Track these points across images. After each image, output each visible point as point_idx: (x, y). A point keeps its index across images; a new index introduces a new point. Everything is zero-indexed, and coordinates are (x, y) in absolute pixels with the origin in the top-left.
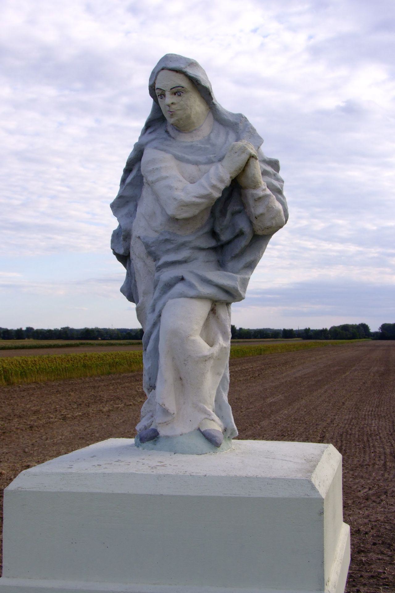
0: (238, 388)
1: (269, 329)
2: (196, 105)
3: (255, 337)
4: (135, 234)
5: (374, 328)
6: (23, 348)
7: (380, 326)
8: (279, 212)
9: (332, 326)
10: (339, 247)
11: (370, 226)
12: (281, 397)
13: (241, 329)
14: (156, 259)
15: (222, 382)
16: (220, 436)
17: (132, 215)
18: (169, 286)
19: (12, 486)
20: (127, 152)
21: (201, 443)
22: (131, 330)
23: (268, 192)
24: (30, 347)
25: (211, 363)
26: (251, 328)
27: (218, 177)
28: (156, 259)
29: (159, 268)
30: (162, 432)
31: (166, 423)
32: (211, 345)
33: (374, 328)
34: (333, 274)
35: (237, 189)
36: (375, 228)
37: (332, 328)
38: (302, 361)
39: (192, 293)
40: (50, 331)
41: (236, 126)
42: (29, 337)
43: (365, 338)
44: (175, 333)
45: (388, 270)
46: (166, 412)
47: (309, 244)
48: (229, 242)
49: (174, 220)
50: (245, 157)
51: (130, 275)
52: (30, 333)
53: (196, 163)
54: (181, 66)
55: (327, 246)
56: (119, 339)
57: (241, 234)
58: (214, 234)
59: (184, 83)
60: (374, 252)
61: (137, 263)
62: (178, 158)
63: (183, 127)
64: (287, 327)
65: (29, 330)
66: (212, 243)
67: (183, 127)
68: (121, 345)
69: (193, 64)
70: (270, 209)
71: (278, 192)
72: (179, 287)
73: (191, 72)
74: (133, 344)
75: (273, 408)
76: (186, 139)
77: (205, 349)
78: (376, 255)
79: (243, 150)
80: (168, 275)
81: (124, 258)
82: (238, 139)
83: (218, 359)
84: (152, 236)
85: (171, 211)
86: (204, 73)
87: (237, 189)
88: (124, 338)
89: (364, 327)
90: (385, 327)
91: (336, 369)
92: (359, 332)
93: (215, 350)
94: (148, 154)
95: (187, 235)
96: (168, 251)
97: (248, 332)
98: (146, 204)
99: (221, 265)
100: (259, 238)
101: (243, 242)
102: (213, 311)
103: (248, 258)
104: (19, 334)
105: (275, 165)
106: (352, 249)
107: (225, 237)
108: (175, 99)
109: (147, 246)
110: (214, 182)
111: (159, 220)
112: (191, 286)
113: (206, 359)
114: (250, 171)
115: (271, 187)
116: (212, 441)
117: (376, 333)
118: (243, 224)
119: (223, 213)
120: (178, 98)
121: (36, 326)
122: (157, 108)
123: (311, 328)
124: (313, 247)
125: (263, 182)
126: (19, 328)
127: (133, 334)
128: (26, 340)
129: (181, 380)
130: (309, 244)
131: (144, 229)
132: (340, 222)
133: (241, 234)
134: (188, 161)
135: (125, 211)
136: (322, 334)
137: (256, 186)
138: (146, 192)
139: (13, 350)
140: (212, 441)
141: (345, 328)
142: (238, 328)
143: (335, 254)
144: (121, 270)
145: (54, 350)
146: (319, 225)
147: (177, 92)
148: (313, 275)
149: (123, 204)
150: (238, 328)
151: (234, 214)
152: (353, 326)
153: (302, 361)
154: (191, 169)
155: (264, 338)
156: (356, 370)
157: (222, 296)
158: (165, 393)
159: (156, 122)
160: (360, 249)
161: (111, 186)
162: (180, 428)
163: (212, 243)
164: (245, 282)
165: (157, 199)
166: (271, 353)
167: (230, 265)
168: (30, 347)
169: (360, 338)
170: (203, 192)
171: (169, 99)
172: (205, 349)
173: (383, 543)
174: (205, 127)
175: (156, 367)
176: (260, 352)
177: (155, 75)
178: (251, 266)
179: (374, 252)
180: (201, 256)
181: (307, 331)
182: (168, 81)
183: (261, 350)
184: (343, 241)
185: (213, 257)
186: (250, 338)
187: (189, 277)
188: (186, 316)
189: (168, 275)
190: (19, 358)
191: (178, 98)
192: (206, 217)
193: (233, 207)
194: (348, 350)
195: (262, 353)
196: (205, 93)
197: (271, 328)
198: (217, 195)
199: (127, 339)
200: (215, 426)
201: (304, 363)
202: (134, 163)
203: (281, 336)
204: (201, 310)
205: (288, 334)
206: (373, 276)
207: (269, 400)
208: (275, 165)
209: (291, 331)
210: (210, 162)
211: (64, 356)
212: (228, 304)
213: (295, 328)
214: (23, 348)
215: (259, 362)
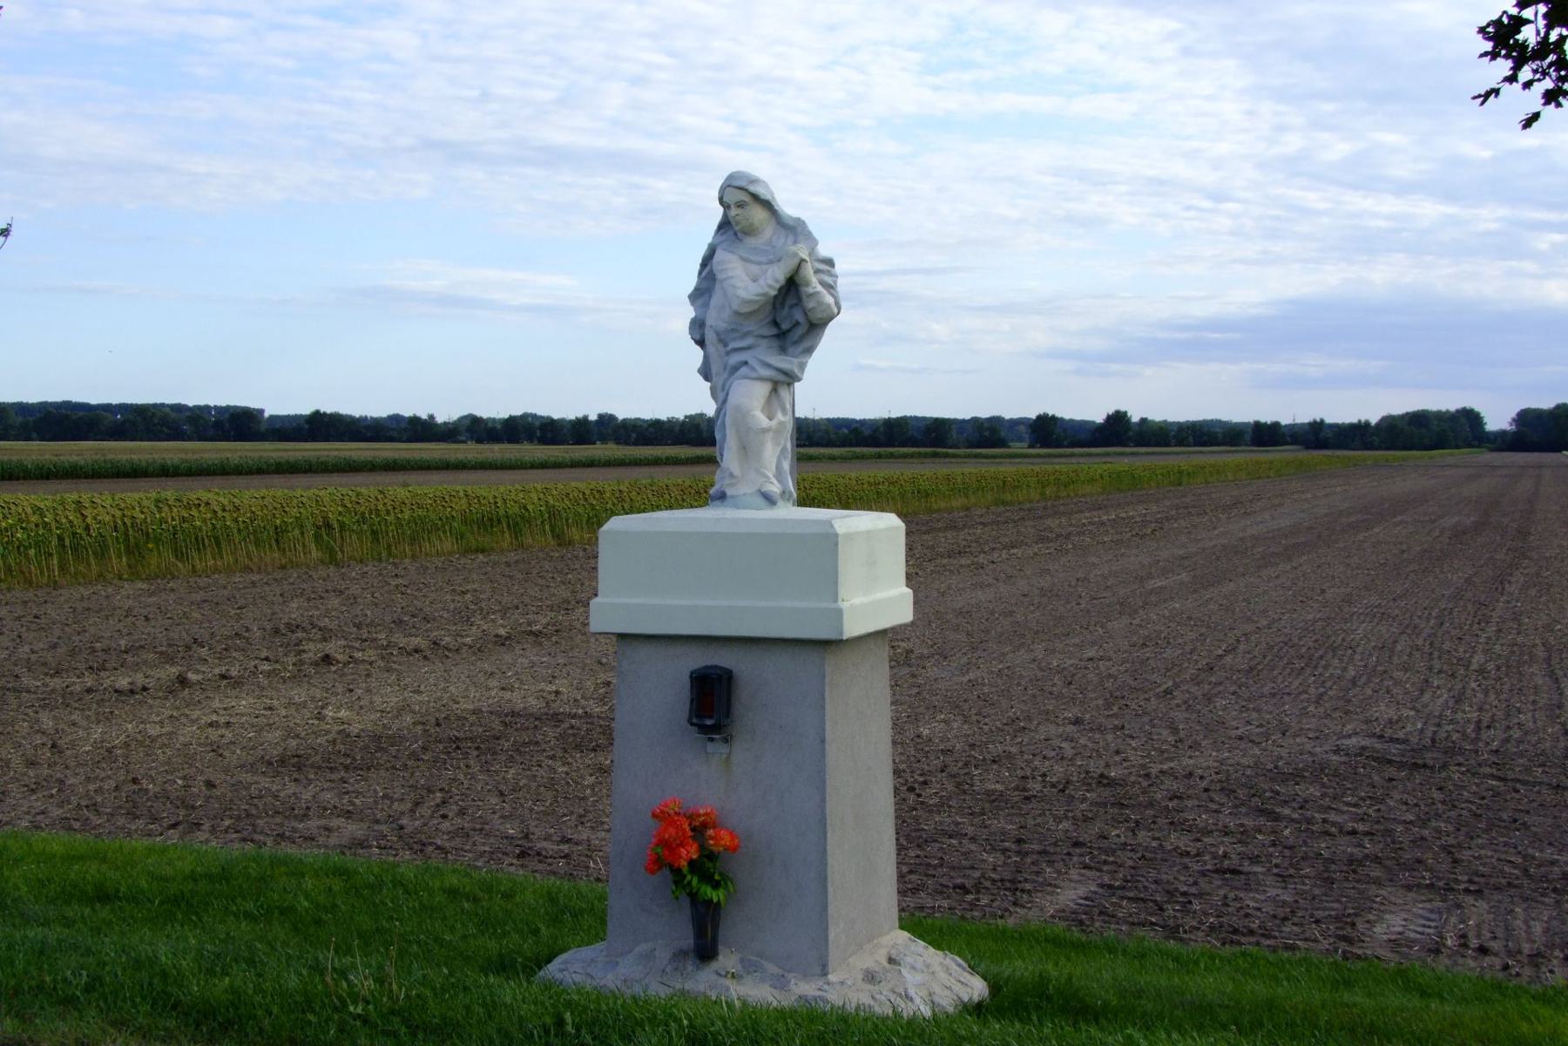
0: (1093, 559)
1: (1219, 422)
2: (758, 215)
3: (1181, 443)
4: (709, 322)
5: (1498, 419)
6: (591, 464)
7: (1513, 414)
8: (829, 306)
9: (1385, 413)
10: (1391, 205)
11: (1468, 149)
12: (1184, 576)
13: (1144, 421)
14: (726, 345)
15: (784, 450)
16: (777, 497)
17: (706, 305)
18: (735, 369)
19: (606, 527)
20: (702, 250)
21: (760, 501)
22: (863, 422)
23: (820, 288)
24: (609, 464)
25: (771, 434)
26: (1170, 419)
27: (775, 277)
28: (726, 345)
29: (728, 353)
30: (729, 493)
31: (732, 485)
32: (770, 419)
33: (1498, 419)
34: (1382, 276)
35: (792, 286)
36: (1486, 154)
37: (1384, 419)
38: (1276, 501)
39: (754, 375)
40: (656, 424)
41: (795, 229)
42: (604, 440)
43: (1470, 446)
44: (738, 408)
45: (1529, 266)
46: (732, 475)
47: (1313, 199)
48: (789, 331)
49: (737, 313)
50: (796, 261)
51: (706, 357)
52: (607, 429)
53: (759, 263)
54: (742, 184)
55: (1359, 202)
56: (829, 444)
57: (797, 324)
58: (775, 323)
59: (746, 198)
60: (1489, 217)
61: (711, 349)
62: (744, 260)
63: (750, 231)
64: (1267, 417)
65: (606, 420)
66: (774, 331)
67: (750, 231)
68: (832, 458)
69: (755, 181)
70: (820, 303)
71: (830, 288)
72: (744, 370)
73: (752, 188)
74: (862, 457)
75: (1153, 598)
76: (751, 241)
77: (763, 421)
78: (1493, 226)
79: (795, 255)
80: (735, 359)
81: (701, 343)
82: (795, 242)
83: (778, 431)
84: (722, 325)
85: (735, 307)
86: (766, 186)
87: (792, 286)
88: (844, 443)
89: (1470, 418)
90: (1527, 419)
91: (1352, 519)
92: (1461, 429)
93: (774, 423)
94: (720, 255)
95: (750, 326)
96: (734, 339)
97: (1161, 428)
98: (716, 300)
99: (783, 350)
100: (815, 326)
101: (800, 331)
102: (775, 390)
103: (806, 344)
104: (582, 431)
105: (830, 262)
106: (1429, 210)
107: (785, 326)
108: (739, 211)
109: (718, 334)
110: (770, 282)
111: (727, 314)
112: (753, 369)
113: (765, 431)
114: (802, 271)
115: (822, 283)
116: (769, 500)
117: (1503, 433)
118: (798, 316)
119: (783, 305)
120: (745, 210)
121: (623, 412)
122: (725, 215)
123: (1328, 420)
124: (1322, 206)
125: (814, 280)
126: (580, 415)
127: (867, 433)
128: (598, 445)
129: (744, 449)
130: (1313, 199)
131: (715, 320)
132: (1391, 138)
133: (797, 324)
134: (752, 262)
135: (701, 301)
136: (1355, 436)
137: (808, 284)
138: (717, 286)
139: (567, 470)
140: (769, 500)
141: (1419, 419)
142: (1135, 419)
143: (1382, 224)
144: (697, 354)
145: (668, 469)
146: (1338, 149)
147: (740, 205)
148: (1326, 279)
149: (701, 294)
150: (1135, 419)
151: (792, 307)
152: (1440, 416)
153: (1276, 501)
154: (754, 269)
155: (1204, 444)
156: (1401, 522)
157: (781, 377)
158: (730, 459)
159: (725, 225)
160: (1451, 210)
161: (691, 281)
162: (744, 489)
163: (774, 331)
164: (802, 367)
165: (725, 294)
166: (1207, 482)
167: (791, 350)
168: (609, 464)
169: (1457, 447)
170: (761, 291)
171: (733, 212)
172: (763, 421)
173: (1222, 789)
174: (769, 231)
175: (724, 437)
176: (1179, 478)
177: (722, 190)
178: (809, 351)
179: (1489, 217)
180: (764, 343)
181: (1317, 427)
182: (732, 197)
183: (1180, 472)
184: (1403, 189)
185: (775, 343)
186: (1167, 445)
187: (752, 362)
188: (751, 395)
189: (735, 359)
190: (582, 486)
191: (745, 210)
192: (769, 307)
193: (790, 301)
194: (1410, 475)
195: (1185, 480)
196: (768, 205)
197: (1224, 419)
198: (773, 293)
199: (851, 445)
200: (774, 488)
201: (1281, 505)
202: (707, 261)
203: (1248, 437)
204: (762, 390)
205: (1266, 435)
206: (1491, 284)
207: (1151, 584)
208: (830, 262)
209: (1276, 426)
210: (770, 262)
211: (688, 483)
212: (789, 385)
213: (1285, 420)
214: (591, 464)
215: (1168, 503)
